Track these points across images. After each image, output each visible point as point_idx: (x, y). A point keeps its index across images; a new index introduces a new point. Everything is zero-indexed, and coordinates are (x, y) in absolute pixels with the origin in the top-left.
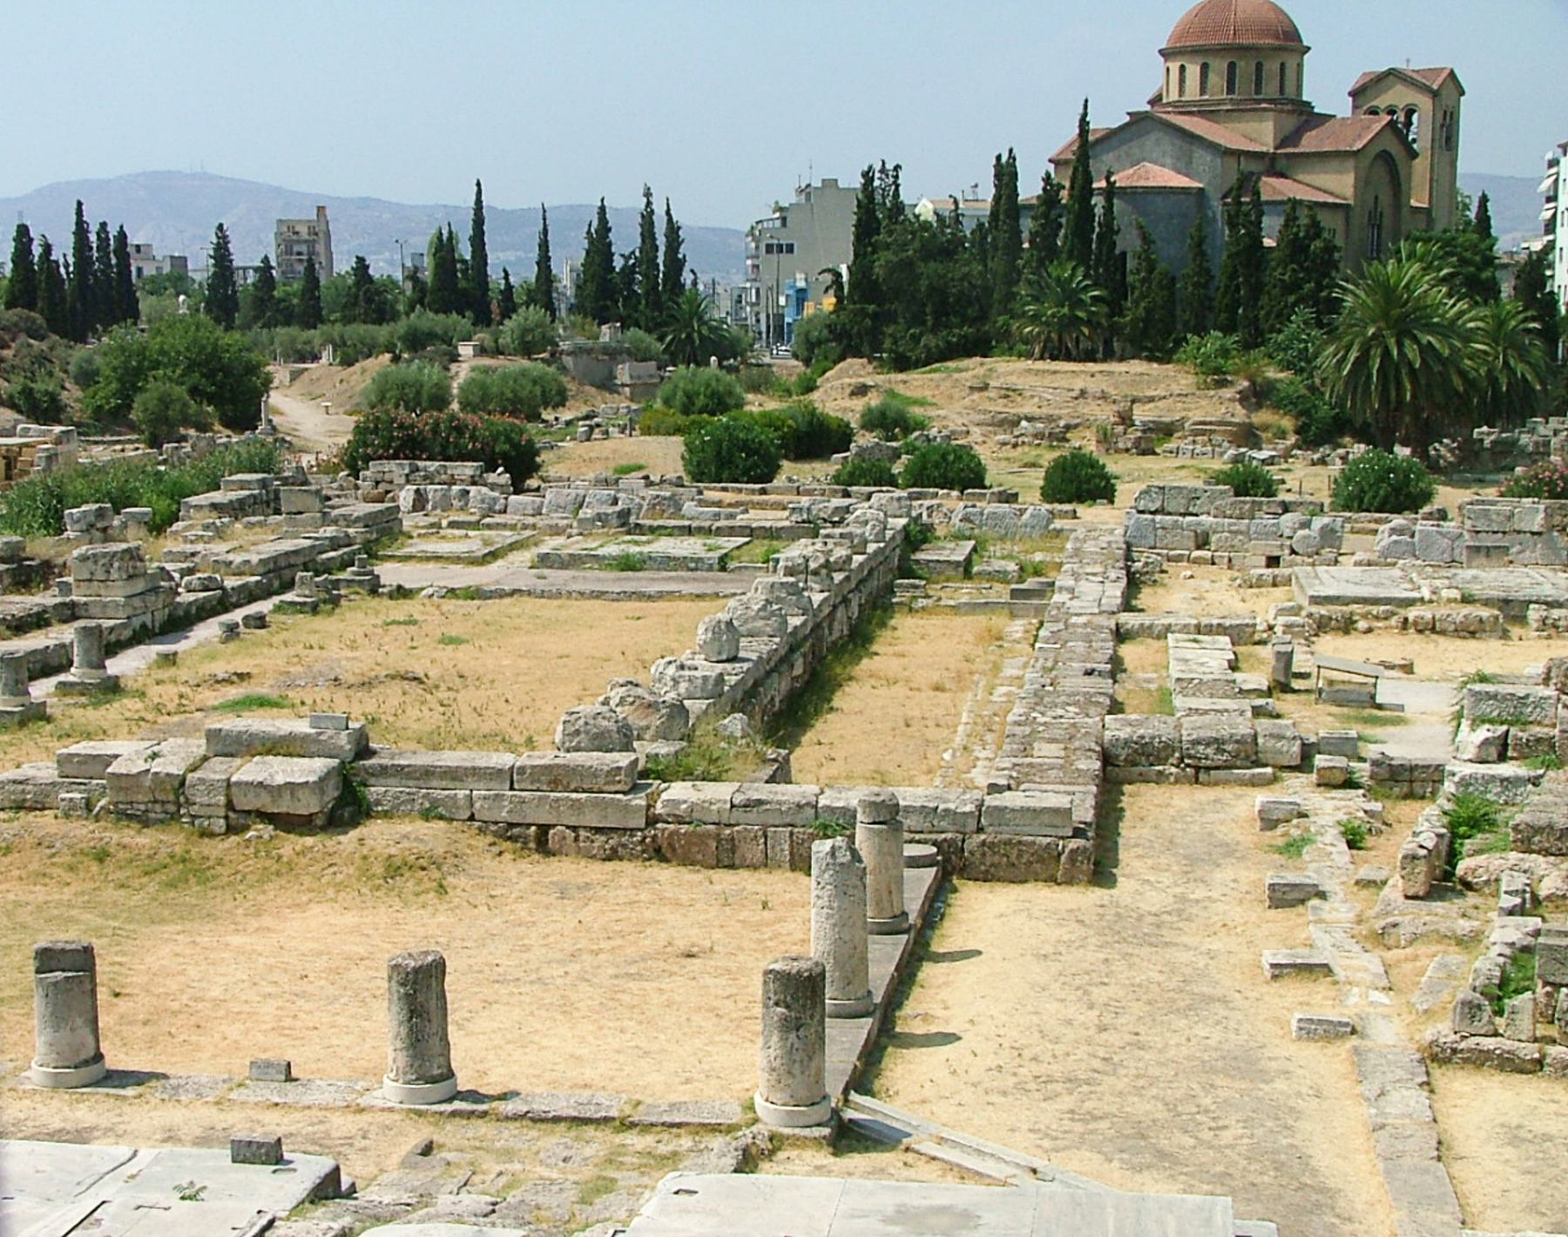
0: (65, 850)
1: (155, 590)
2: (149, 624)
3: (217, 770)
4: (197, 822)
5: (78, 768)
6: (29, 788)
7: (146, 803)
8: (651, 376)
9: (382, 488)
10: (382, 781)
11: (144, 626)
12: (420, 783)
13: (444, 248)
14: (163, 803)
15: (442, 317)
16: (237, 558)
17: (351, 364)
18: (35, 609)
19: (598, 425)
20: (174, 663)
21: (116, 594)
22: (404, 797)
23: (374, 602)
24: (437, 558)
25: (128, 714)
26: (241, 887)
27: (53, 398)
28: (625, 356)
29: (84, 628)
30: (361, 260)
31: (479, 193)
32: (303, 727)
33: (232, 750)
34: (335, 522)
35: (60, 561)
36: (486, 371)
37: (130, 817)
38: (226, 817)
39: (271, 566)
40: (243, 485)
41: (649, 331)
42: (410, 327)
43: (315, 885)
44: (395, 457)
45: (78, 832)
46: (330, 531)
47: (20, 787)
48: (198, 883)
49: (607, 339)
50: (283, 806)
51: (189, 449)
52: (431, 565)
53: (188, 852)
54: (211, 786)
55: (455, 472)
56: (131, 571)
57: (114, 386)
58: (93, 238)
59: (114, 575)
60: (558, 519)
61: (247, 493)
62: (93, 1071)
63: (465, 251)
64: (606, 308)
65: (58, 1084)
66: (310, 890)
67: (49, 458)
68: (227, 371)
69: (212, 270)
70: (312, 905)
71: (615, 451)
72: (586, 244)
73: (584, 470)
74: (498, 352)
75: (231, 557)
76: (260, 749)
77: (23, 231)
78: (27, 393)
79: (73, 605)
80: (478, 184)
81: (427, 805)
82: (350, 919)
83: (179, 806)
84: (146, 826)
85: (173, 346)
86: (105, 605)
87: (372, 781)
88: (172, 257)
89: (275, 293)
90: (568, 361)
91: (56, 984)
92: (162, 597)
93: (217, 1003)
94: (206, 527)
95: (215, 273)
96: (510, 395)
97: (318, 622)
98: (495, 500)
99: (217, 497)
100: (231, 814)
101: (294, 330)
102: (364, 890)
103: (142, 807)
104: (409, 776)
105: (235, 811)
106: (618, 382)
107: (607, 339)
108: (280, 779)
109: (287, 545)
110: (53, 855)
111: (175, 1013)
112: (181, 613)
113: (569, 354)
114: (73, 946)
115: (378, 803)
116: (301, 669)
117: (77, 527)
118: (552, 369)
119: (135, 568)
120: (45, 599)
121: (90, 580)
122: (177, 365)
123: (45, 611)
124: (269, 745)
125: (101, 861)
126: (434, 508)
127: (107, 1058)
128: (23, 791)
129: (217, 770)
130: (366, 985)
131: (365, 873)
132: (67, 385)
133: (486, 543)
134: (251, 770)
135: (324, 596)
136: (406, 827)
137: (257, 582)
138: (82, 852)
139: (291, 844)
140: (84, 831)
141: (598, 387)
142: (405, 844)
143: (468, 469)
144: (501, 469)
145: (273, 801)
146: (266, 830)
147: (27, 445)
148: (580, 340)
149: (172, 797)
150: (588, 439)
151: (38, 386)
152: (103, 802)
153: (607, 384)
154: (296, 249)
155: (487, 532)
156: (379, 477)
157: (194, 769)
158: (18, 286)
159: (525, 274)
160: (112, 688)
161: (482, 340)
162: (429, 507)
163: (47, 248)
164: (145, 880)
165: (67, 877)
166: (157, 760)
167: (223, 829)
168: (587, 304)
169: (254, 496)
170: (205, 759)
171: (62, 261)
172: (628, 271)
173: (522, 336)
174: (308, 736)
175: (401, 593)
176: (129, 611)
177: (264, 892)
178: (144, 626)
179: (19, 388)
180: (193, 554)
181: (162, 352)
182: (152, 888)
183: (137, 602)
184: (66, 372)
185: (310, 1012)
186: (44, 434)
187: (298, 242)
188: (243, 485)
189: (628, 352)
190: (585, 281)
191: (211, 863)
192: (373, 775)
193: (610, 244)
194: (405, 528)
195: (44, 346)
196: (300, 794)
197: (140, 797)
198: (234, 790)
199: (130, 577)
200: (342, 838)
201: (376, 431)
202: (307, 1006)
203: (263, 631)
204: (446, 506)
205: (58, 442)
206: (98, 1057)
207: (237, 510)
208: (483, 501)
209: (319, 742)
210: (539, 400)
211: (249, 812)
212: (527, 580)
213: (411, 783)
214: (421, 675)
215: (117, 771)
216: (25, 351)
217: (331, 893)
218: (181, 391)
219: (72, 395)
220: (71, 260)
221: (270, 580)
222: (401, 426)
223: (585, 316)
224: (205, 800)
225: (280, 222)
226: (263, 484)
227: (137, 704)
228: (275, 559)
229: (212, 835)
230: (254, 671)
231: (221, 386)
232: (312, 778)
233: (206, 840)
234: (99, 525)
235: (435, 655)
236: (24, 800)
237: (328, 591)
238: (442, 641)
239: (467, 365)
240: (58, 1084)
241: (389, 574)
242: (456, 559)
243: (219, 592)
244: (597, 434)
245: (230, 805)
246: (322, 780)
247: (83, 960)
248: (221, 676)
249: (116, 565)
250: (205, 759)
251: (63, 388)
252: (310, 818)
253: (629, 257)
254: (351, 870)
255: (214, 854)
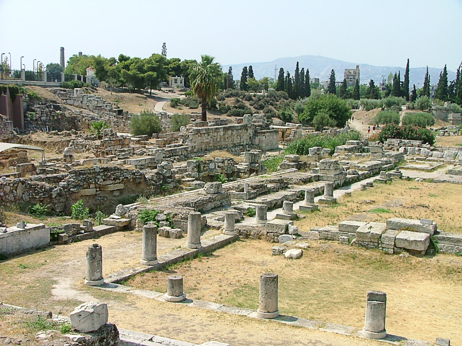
0: (342, 254)
1: (341, 173)
2: (339, 183)
3: (391, 234)
4: (384, 249)
5: (344, 229)
6: (329, 233)
7: (368, 242)
8: (459, 118)
9: (390, 146)
10: (443, 242)
11: (338, 184)
12: (456, 244)
13: (397, 79)
14: (374, 242)
15: (396, 98)
16: (361, 166)
17: (369, 110)
18: (309, 177)
19: (447, 131)
20: (350, 196)
21: (332, 174)
22: (450, 248)
23: (401, 181)
24: (417, 169)
25: (343, 211)
26: (399, 272)
27: (290, 116)
28: (451, 112)
29: (328, 184)
30: (372, 81)
31: (408, 62)
32: (417, 222)
33: (394, 228)
34: (386, 156)
35: (309, 163)
36: (410, 114)
37: (363, 246)
38: (394, 249)
39: (371, 168)
40: (352, 144)
41: (458, 104)
42: (388, 100)
43: (424, 274)
44: (394, 138)
45: (346, 249)
46: (385, 159)
47: (327, 233)
48: (385, 269)
49: (446, 106)
50: (412, 247)
51: (329, 132)
52: (415, 171)
53: (381, 259)
54: (390, 239)
55: (413, 143)
56: (336, 168)
57: (309, 113)
58: (300, 72)
59: (331, 168)
60: (448, 159)
61: (354, 146)
62: (383, 334)
63: (402, 79)
64: (445, 97)
65: (372, 337)
66: (422, 275)
67: (295, 133)
68: (340, 110)
69: (329, 83)
70: (424, 280)
71: (456, 140)
72: (439, 78)
73: (446, 145)
74: (413, 108)
75: (359, 165)
76: (404, 228)
77: (282, 70)
78: (283, 114)
79: (319, 176)
80: (408, 60)
81: (458, 251)
82: (439, 287)
83: (379, 244)
84: (367, 249)
85: (326, 103)
86: (328, 177)
87: (439, 242)
88: (315, 79)
89: (347, 89)
90: (434, 112)
91: (374, 305)
92: (343, 175)
93: (408, 312)
94: (346, 155)
95: (330, 83)
96: (418, 121)
97: (387, 186)
98: (429, 152)
99: (345, 146)
100: (395, 248)
101: (352, 100)
102: (440, 277)
103: (367, 243)
104: (452, 241)
105: (396, 247)
106: (449, 119)
107: (446, 106)
108: (412, 239)
109: (374, 162)
110: (339, 255)
111: (395, 314)
112: (348, 181)
113: (434, 110)
114: (380, 293)
115: (441, 249)
116: (389, 201)
117: (312, 153)
118: (430, 114)
119: (337, 167)
120: (309, 174)
121: (324, 169)
122: (326, 108)
123: (311, 178)
124: (407, 227)
125: (354, 259)
126: (410, 154)
127: (387, 331)
128: (328, 234)
129: (391, 234)
130: (455, 312)
131: (439, 271)
132: (294, 113)
133: (431, 166)
134: (403, 235)
135: (388, 178)
136: (451, 258)
137: (367, 173)
138: (348, 255)
139: (415, 260)
140: (348, 249)
141: (443, 120)
142: (453, 264)
143: (417, 143)
144: (427, 143)
145: (409, 245)
146: (407, 254)
147: (288, 129)
148: (438, 106)
149: (376, 241)
150: (444, 135)
151: (286, 112)
152: (354, 240)
153: (445, 119)
154: (350, 77)
155: (430, 162)
156: (390, 143)
157: (384, 232)
158: (279, 85)
159: (420, 86)
160: (335, 202)
161: (409, 105)
162: (408, 153)
163: (289, 75)
164: (368, 266)
165: (344, 262)
166: (372, 229)
167: (392, 253)
168: (438, 95)
169: (355, 147)
170: (386, 230)
171: (292, 78)
172: (452, 86)
173: (421, 104)
174: (419, 225)
175: (409, 179)
176: (335, 179)
177: (407, 274)
178: (338, 184)
179: (281, 113)
180: (348, 163)
181: (322, 104)
182: (371, 269)
183: (337, 176)
184: (293, 109)
185: (440, 320)
186: (293, 126)
187: (351, 75)
188: (352, 144)
189: (452, 110)
190: (438, 89)
191: (389, 263)
192: (440, 240)
193: (447, 78)
194: (405, 159)
195: (288, 101)
196: (419, 244)
197: (366, 240)
198: (396, 241)
199: (335, 169)
200: (431, 259)
201: (389, 130)
202: (438, 317)
203: (372, 188)
204: (413, 154)
205: (297, 128)
206: (384, 330)
207: (350, 150)
208: (425, 153)
209: (423, 228)
210: (426, 123)
211: (401, 248)
212: (447, 178)
213: (452, 243)
214: (428, 206)
215: (360, 231)
216: (283, 103)
217: (429, 277)
218: (327, 116)
219: (295, 115)
220: (294, 78)
221: (370, 173)
222: (396, 129)
223: (440, 99)
224: (387, 243)
225: (346, 70)
226: (358, 144)
227: (344, 208)
228: (372, 166)
229: (389, 254)
230: (376, 200)
231: (338, 115)
232: (423, 239)
233: (387, 255)
234: (318, 153)
235: (429, 199)
236: (328, 237)
237: (389, 177)
238: (430, 195)
239: (404, 112)
240: (372, 337)
241: (405, 173)
242: (423, 170)
243: (357, 175)
244: (446, 134)
245: (395, 245)
246: (425, 240)
247: (383, 298)
248: (368, 201)
249: (332, 165)
250: (386, 230)
251: (293, 113)
252: (420, 252)
253: (453, 82)
254: (435, 270)
255: (390, 260)
